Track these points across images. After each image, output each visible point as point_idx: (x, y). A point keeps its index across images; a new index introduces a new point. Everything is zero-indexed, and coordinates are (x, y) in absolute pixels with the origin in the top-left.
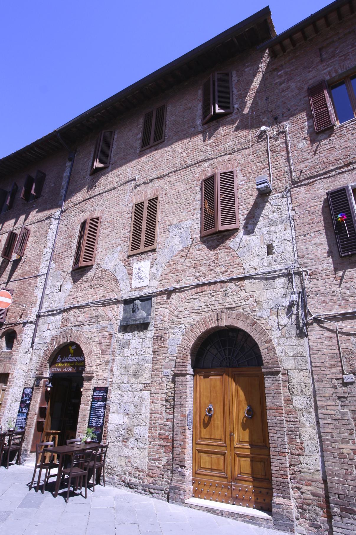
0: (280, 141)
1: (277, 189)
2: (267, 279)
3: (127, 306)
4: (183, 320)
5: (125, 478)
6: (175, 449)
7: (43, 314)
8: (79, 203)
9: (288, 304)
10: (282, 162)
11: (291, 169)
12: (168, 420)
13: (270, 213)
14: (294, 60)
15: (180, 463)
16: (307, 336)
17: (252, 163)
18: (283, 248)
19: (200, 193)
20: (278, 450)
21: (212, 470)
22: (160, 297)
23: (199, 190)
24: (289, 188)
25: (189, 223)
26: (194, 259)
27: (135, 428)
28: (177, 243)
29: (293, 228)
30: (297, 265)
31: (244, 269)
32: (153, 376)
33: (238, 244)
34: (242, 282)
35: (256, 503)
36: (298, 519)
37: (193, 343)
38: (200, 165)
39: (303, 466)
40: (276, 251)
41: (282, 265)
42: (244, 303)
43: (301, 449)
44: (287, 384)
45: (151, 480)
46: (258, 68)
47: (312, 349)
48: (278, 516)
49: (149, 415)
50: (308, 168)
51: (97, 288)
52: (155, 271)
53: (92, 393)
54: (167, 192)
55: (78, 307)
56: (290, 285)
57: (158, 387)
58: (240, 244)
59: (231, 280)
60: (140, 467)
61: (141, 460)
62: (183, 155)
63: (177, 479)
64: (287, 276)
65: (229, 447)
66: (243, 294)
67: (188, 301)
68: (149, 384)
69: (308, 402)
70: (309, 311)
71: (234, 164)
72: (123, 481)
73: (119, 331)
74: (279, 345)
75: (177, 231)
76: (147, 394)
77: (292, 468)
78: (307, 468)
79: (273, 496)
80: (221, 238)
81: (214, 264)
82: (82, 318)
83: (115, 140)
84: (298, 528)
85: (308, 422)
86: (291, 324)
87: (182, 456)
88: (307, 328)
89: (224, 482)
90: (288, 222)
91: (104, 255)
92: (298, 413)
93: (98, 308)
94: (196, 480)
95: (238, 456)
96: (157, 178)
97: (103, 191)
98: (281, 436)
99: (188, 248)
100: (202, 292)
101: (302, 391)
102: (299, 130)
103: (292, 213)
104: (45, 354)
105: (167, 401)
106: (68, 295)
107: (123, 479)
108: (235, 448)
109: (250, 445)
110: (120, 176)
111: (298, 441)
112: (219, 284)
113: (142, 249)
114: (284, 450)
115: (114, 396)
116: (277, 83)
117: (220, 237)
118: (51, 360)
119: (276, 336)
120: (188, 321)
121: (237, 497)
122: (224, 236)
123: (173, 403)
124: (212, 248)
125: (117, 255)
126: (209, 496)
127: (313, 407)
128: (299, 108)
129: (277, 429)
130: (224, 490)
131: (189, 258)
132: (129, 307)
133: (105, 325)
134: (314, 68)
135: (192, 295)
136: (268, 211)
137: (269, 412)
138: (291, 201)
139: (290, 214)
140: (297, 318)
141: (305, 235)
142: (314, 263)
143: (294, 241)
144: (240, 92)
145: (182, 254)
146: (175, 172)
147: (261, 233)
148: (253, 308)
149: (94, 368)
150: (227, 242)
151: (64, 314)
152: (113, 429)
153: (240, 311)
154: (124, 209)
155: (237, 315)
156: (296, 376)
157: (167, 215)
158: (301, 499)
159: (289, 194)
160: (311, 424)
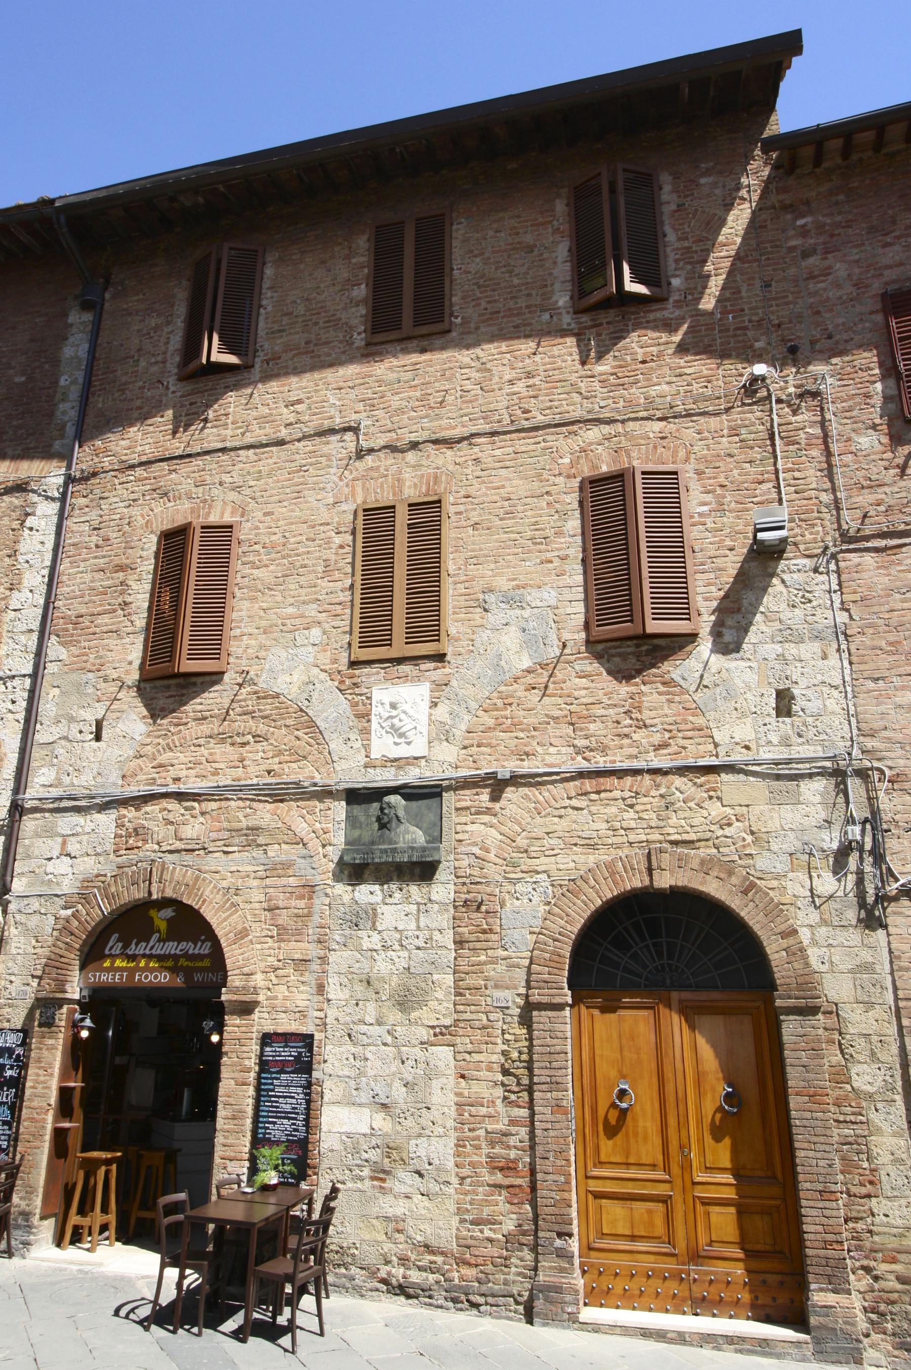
0: (805, 417)
1: (802, 547)
2: (778, 777)
3: (357, 810)
4: (543, 863)
5: (389, 1273)
6: (540, 1193)
7: (35, 803)
8: (141, 464)
9: (835, 845)
10: (812, 475)
11: (836, 501)
12: (513, 1122)
13: (783, 606)
14: (841, 197)
15: (557, 1228)
16: (886, 927)
17: (729, 459)
18: (819, 703)
19: (577, 514)
20: (820, 1187)
21: (633, 1238)
22: (467, 792)
23: (576, 505)
24: (833, 549)
25: (549, 596)
26: (569, 700)
27: (413, 1142)
28: (515, 648)
29: (845, 655)
30: (856, 752)
31: (716, 745)
32: (461, 1008)
33: (697, 675)
34: (712, 777)
35: (753, 1306)
36: (867, 1336)
37: (579, 926)
38: (575, 433)
39: (877, 1220)
40: (803, 710)
41: (819, 748)
42: (720, 833)
43: (871, 1183)
44: (836, 1036)
45: (470, 1272)
46: (738, 187)
47: (899, 957)
48: (824, 1334)
49: (454, 1108)
50: (882, 508)
51: (244, 744)
52: (446, 718)
53: (256, 1048)
54: (471, 491)
55: (180, 796)
56: (841, 799)
57: (478, 1035)
58: (702, 676)
59: (682, 771)
60: (434, 1242)
61: (436, 1220)
62: (515, 389)
63: (550, 1268)
64: (831, 775)
65: (678, 1182)
66: (715, 810)
67: (557, 813)
68: (446, 1027)
69: (887, 1078)
70: (889, 869)
71: (675, 452)
72: (384, 1281)
73: (337, 878)
74: (814, 942)
75: (512, 612)
76: (443, 1055)
77: (851, 1225)
78: (887, 1225)
79: (809, 1290)
80: (648, 653)
81: (628, 721)
82: (195, 829)
83: (266, 284)
84: (870, 1354)
85: (888, 1124)
86: (846, 895)
87: (564, 1211)
88: (884, 909)
89: (671, 1265)
90: (833, 637)
91: (266, 648)
92: (864, 1104)
93: (255, 805)
94: (592, 1265)
95: (703, 1204)
96: (435, 442)
97: (237, 444)
98: (826, 1155)
99: (550, 667)
100: (598, 792)
101: (873, 1054)
102: (857, 400)
103: (842, 617)
104: (65, 929)
105: (506, 1072)
106: (131, 753)
107: (383, 1274)
108: (694, 1183)
109: (735, 1176)
110: (299, 407)
111: (865, 1165)
112: (647, 777)
113: (399, 648)
114: (833, 1188)
115: (333, 1061)
116: (792, 249)
117: (644, 648)
118: (86, 950)
119: (807, 922)
120: (562, 867)
121: (704, 1298)
122: (656, 648)
123: (524, 1079)
124: (623, 675)
125: (308, 654)
126: (629, 1300)
127: (900, 1090)
128: (857, 338)
129: (815, 1139)
130: (668, 1283)
131: (554, 695)
132: (366, 811)
133: (283, 858)
134: (898, 238)
135: (570, 798)
136: (776, 598)
137: (794, 1102)
138: (840, 584)
139: (837, 620)
140: (860, 882)
141: (878, 679)
142: (900, 752)
143: (849, 689)
144: (686, 244)
145: (530, 679)
146: (493, 434)
147: (759, 657)
148: (744, 846)
149: (259, 979)
150: (666, 666)
151: (124, 811)
152: (337, 1146)
153: (708, 851)
154: (325, 516)
155: (703, 862)
156: (858, 1018)
157: (476, 560)
158: (873, 1291)
159: (833, 567)
160: (895, 1127)
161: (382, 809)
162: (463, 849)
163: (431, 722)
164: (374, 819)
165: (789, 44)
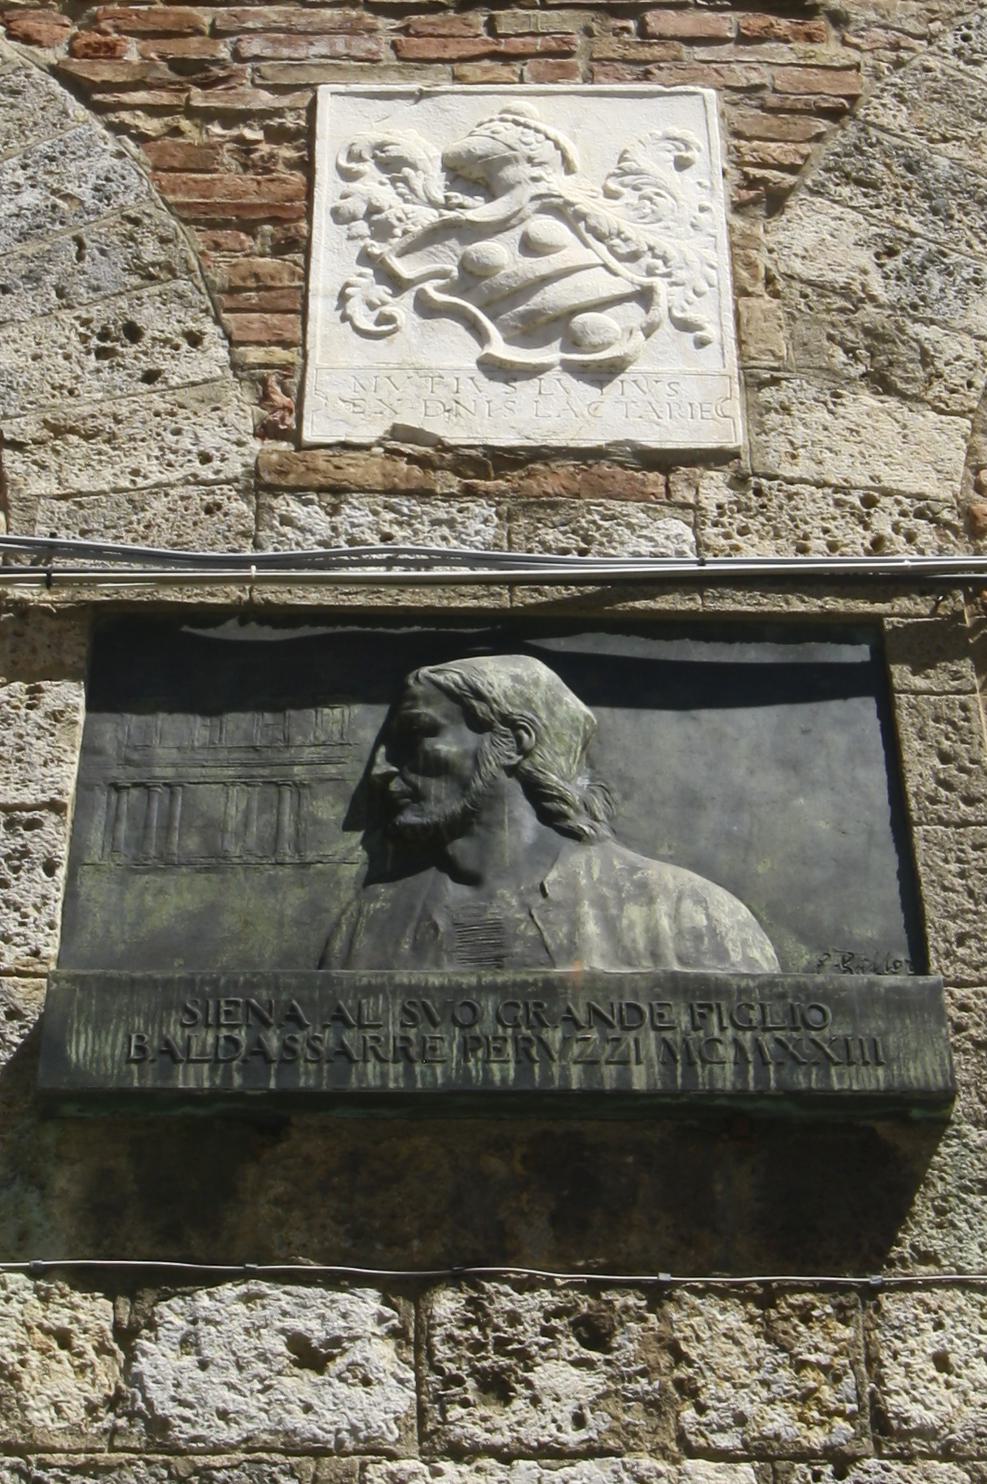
3: (175, 738)
161: (405, 738)
163: (754, 279)
164: (330, 809)
165: (564, 247)
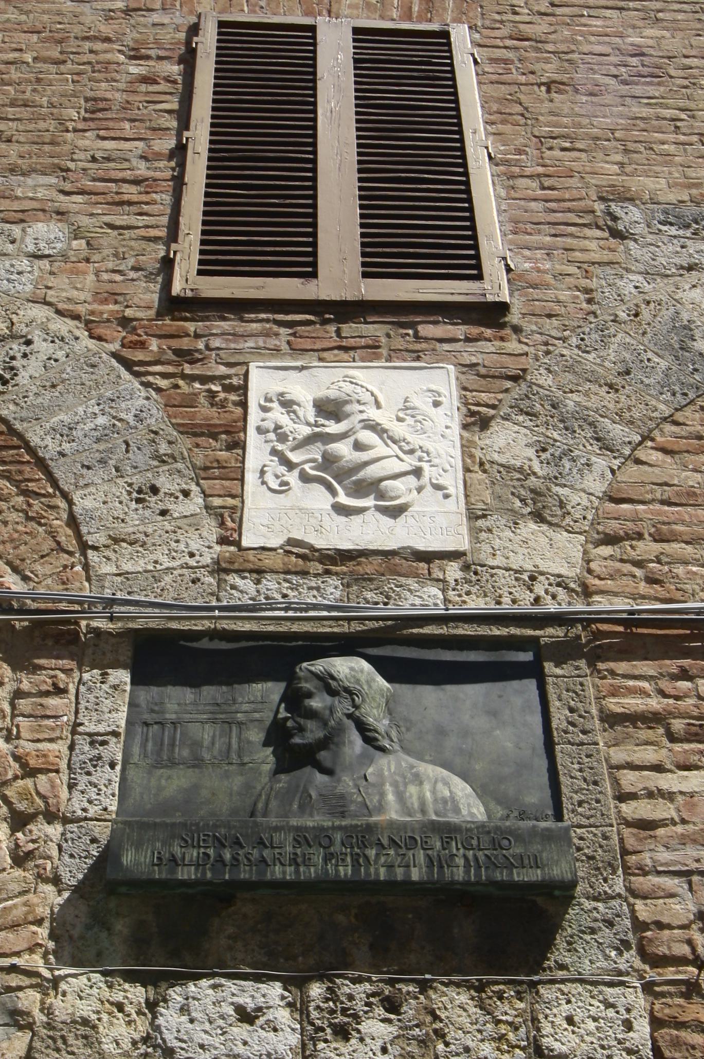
3: (176, 699)
161: (294, 699)
162: (664, 856)
163: (473, 463)
164: (256, 736)
